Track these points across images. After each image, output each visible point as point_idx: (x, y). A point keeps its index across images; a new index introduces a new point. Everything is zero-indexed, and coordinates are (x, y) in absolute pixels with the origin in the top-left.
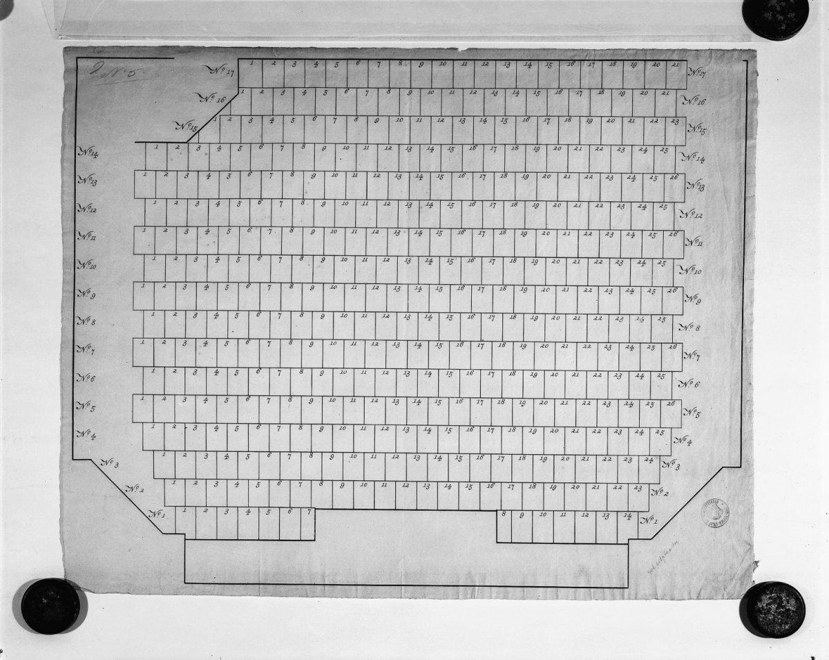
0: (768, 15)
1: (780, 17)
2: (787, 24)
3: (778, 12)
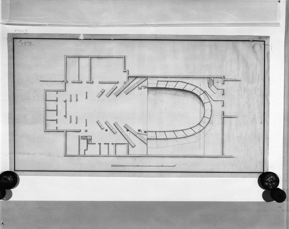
0: (267, 184)
1: (270, 184)
2: (272, 186)
3: (269, 183)
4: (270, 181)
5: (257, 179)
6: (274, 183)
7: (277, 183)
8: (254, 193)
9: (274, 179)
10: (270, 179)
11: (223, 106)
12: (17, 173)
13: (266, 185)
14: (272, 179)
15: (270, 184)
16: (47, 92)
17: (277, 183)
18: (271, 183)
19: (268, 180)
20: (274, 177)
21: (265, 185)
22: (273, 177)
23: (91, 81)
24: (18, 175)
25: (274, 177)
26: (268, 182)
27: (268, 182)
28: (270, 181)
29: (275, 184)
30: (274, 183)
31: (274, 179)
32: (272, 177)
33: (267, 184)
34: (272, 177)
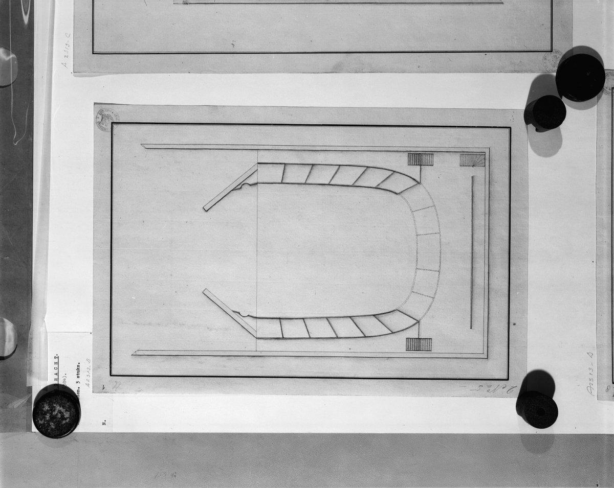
0: (46, 408)
1: (48, 417)
2: (44, 424)
3: (51, 414)
4: (56, 412)
5: (515, 400)
6: (52, 425)
7: (57, 433)
8: (502, 416)
9: (64, 422)
10: (60, 412)
11: (510, 128)
12: (562, 48)
13: (44, 407)
14: (63, 418)
15: (48, 417)
16: (115, 126)
17: (57, 433)
18: (53, 418)
19: (58, 408)
20: (68, 420)
21: (43, 404)
22: (67, 418)
23: (110, 121)
24: (572, 50)
25: (68, 420)
26: (52, 409)
27: (51, 410)
28: (56, 412)
29: (52, 429)
30: (52, 425)
31: (64, 422)
32: (67, 415)
33: (46, 408)
34: (67, 415)
